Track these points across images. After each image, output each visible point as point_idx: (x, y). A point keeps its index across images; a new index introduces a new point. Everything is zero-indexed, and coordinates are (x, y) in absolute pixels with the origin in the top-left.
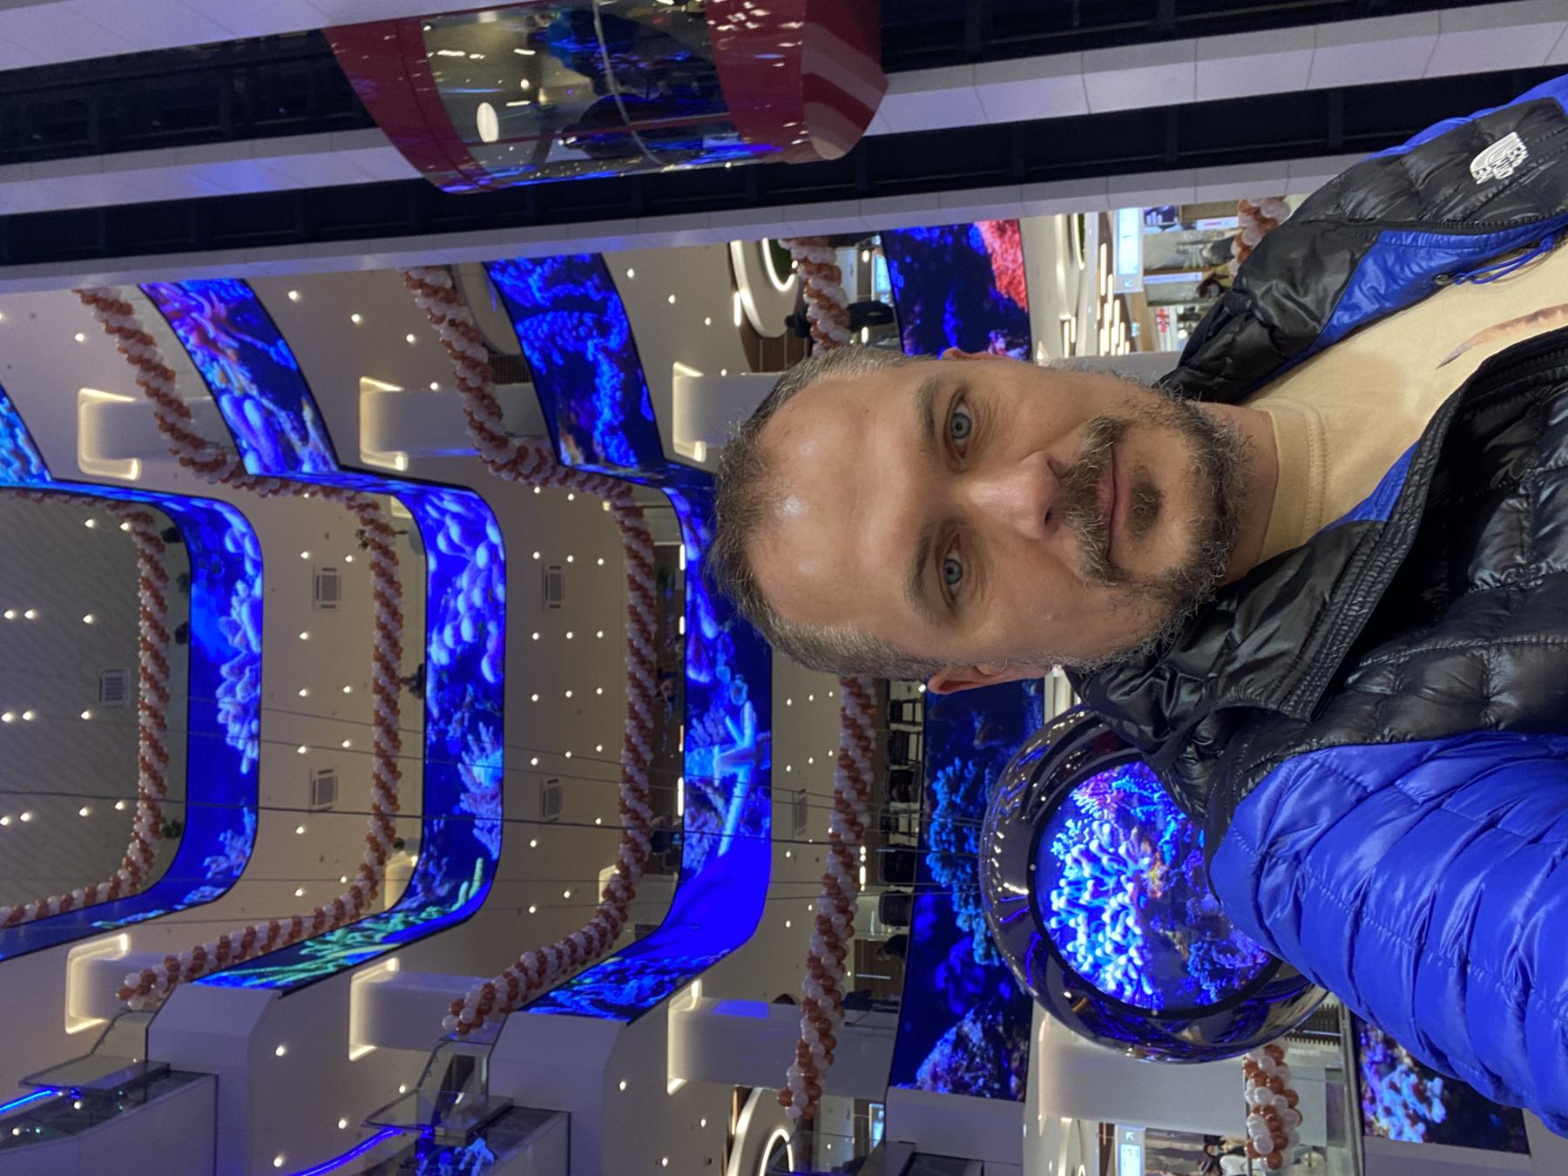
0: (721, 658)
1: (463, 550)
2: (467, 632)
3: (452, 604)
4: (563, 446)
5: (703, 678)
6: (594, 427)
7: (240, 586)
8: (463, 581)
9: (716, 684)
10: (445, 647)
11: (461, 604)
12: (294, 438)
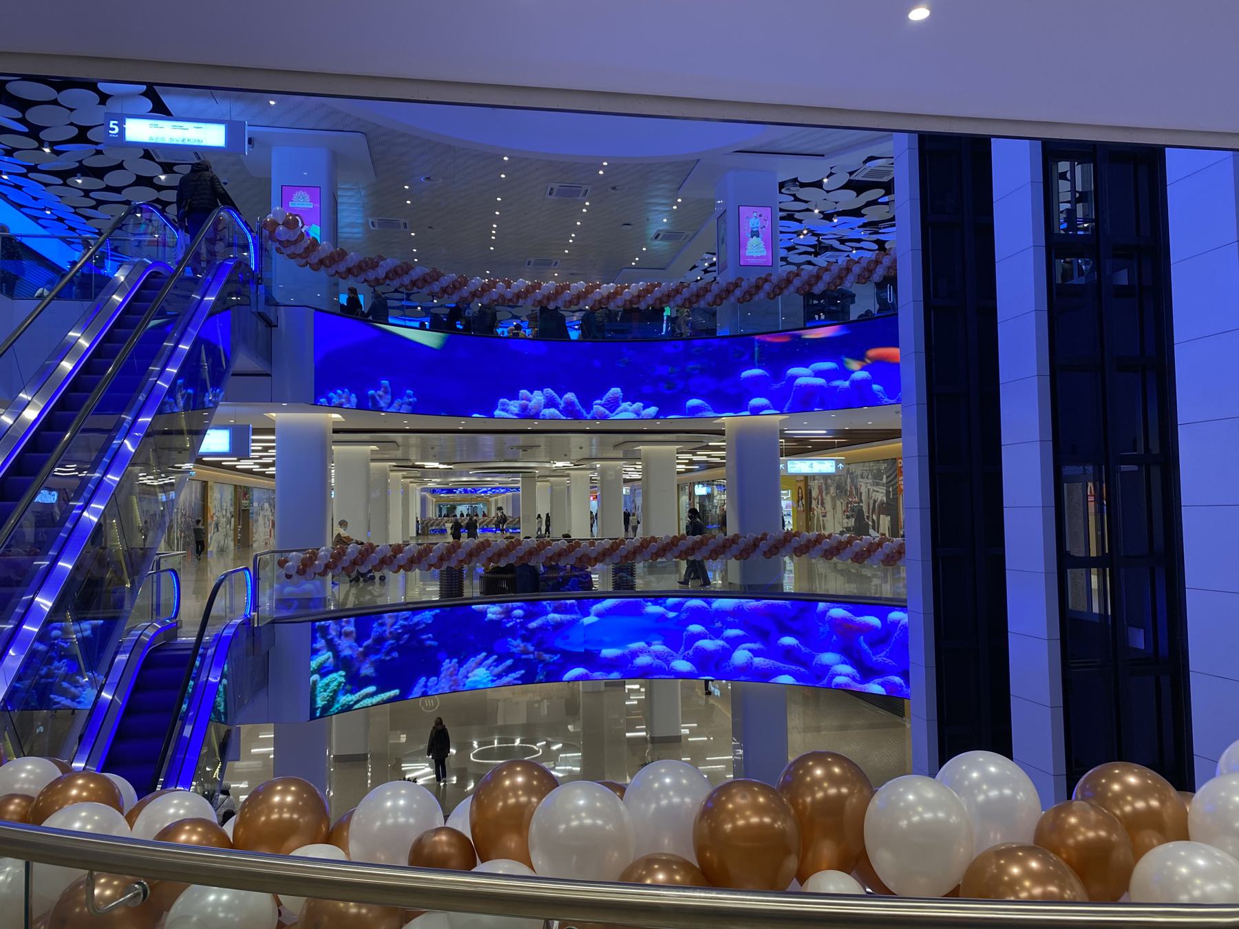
1: (687, 648)
7: (653, 410)
8: (658, 647)
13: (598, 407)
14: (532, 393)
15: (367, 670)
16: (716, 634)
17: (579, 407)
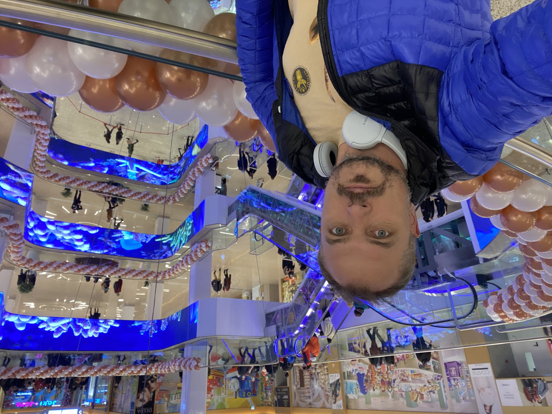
0: (101, 163)
2: (79, 237)
5: (107, 169)
10: (83, 245)
11: (69, 237)
12: (17, 180)
13: (65, 329)
14: (93, 336)
15: (165, 247)
16: (36, 235)
17: (74, 329)
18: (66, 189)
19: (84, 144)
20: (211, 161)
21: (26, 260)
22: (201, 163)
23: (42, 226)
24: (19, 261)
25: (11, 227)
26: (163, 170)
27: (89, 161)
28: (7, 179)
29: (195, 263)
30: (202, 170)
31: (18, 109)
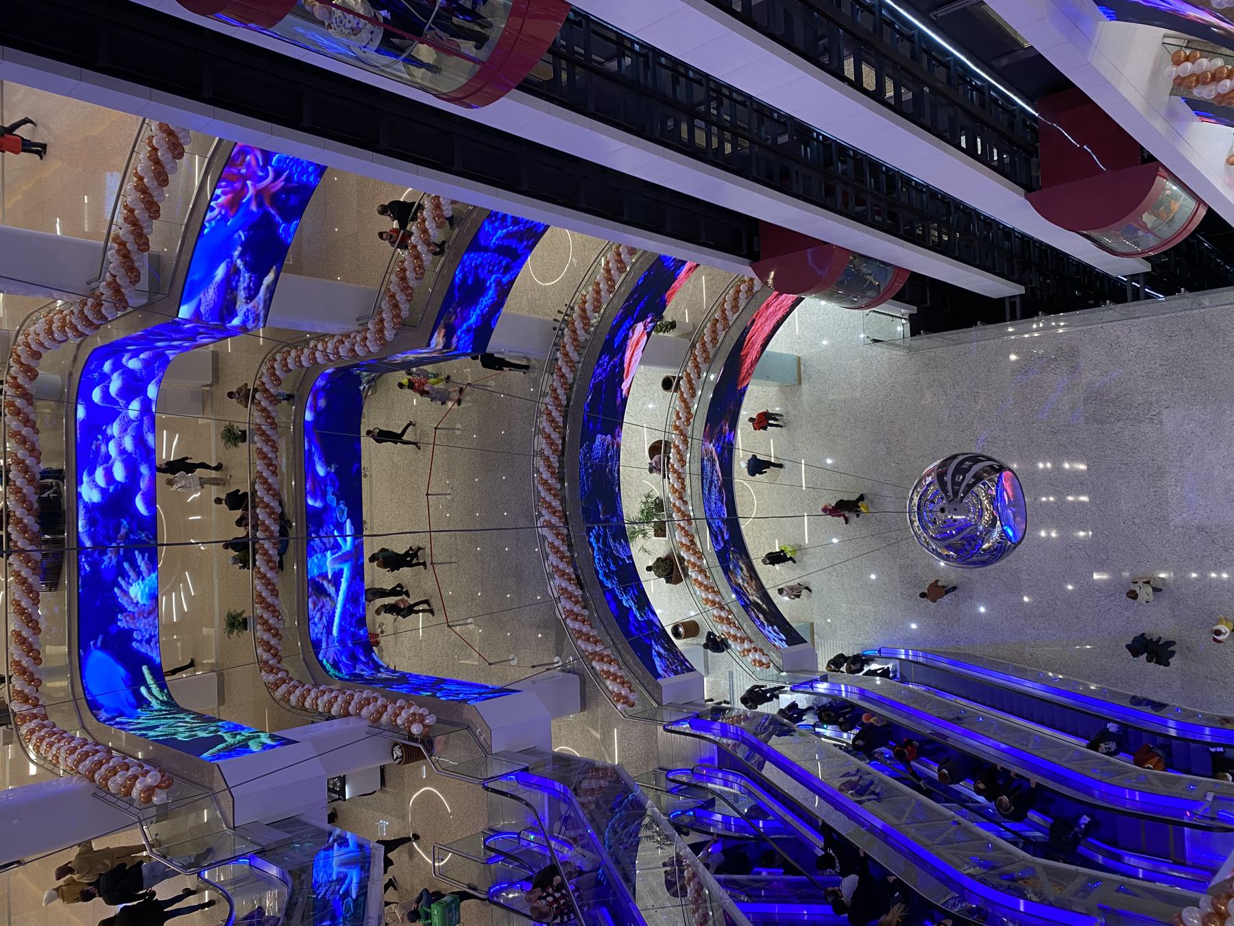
0: (330, 490)
1: (117, 403)
2: (119, 473)
3: (103, 448)
4: (436, 335)
5: (318, 504)
6: (461, 327)
8: (115, 429)
9: (327, 508)
10: (97, 486)
11: (112, 449)
12: (242, 294)
16: (106, 378)
18: (244, 432)
19: (364, 463)
20: (416, 729)
21: (32, 363)
22: (402, 708)
23: (134, 386)
24: (28, 346)
25: (117, 290)
26: (354, 636)
27: (327, 464)
28: (238, 271)
29: (86, 783)
30: (385, 717)
31: (404, 279)
